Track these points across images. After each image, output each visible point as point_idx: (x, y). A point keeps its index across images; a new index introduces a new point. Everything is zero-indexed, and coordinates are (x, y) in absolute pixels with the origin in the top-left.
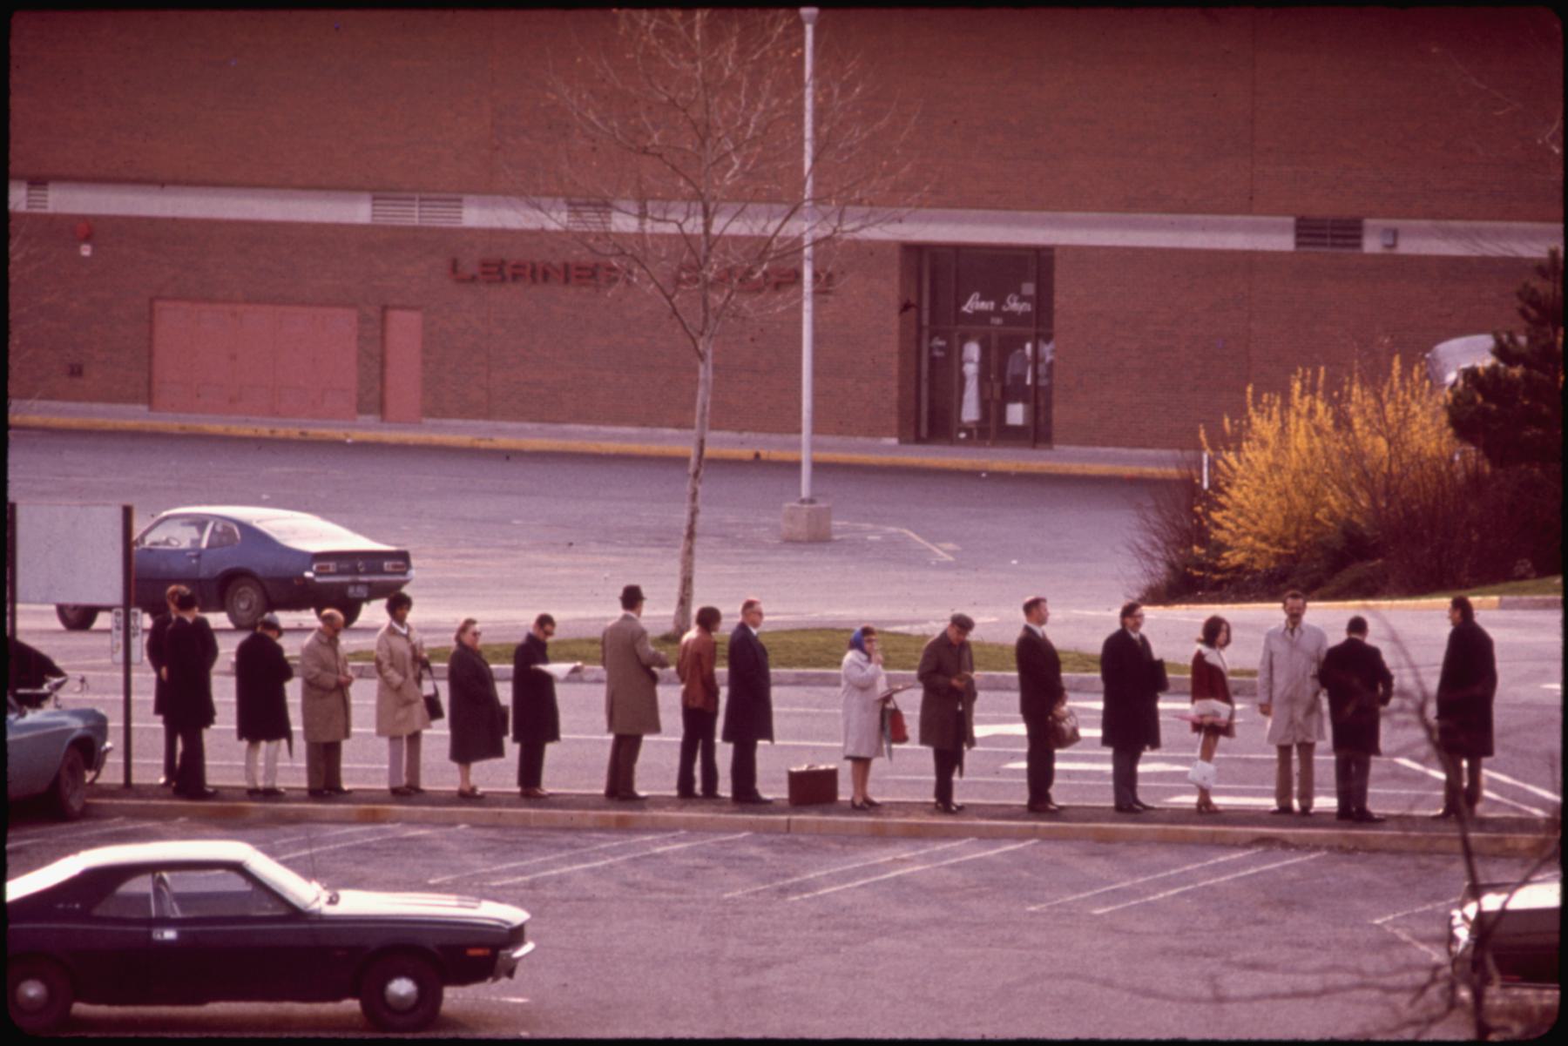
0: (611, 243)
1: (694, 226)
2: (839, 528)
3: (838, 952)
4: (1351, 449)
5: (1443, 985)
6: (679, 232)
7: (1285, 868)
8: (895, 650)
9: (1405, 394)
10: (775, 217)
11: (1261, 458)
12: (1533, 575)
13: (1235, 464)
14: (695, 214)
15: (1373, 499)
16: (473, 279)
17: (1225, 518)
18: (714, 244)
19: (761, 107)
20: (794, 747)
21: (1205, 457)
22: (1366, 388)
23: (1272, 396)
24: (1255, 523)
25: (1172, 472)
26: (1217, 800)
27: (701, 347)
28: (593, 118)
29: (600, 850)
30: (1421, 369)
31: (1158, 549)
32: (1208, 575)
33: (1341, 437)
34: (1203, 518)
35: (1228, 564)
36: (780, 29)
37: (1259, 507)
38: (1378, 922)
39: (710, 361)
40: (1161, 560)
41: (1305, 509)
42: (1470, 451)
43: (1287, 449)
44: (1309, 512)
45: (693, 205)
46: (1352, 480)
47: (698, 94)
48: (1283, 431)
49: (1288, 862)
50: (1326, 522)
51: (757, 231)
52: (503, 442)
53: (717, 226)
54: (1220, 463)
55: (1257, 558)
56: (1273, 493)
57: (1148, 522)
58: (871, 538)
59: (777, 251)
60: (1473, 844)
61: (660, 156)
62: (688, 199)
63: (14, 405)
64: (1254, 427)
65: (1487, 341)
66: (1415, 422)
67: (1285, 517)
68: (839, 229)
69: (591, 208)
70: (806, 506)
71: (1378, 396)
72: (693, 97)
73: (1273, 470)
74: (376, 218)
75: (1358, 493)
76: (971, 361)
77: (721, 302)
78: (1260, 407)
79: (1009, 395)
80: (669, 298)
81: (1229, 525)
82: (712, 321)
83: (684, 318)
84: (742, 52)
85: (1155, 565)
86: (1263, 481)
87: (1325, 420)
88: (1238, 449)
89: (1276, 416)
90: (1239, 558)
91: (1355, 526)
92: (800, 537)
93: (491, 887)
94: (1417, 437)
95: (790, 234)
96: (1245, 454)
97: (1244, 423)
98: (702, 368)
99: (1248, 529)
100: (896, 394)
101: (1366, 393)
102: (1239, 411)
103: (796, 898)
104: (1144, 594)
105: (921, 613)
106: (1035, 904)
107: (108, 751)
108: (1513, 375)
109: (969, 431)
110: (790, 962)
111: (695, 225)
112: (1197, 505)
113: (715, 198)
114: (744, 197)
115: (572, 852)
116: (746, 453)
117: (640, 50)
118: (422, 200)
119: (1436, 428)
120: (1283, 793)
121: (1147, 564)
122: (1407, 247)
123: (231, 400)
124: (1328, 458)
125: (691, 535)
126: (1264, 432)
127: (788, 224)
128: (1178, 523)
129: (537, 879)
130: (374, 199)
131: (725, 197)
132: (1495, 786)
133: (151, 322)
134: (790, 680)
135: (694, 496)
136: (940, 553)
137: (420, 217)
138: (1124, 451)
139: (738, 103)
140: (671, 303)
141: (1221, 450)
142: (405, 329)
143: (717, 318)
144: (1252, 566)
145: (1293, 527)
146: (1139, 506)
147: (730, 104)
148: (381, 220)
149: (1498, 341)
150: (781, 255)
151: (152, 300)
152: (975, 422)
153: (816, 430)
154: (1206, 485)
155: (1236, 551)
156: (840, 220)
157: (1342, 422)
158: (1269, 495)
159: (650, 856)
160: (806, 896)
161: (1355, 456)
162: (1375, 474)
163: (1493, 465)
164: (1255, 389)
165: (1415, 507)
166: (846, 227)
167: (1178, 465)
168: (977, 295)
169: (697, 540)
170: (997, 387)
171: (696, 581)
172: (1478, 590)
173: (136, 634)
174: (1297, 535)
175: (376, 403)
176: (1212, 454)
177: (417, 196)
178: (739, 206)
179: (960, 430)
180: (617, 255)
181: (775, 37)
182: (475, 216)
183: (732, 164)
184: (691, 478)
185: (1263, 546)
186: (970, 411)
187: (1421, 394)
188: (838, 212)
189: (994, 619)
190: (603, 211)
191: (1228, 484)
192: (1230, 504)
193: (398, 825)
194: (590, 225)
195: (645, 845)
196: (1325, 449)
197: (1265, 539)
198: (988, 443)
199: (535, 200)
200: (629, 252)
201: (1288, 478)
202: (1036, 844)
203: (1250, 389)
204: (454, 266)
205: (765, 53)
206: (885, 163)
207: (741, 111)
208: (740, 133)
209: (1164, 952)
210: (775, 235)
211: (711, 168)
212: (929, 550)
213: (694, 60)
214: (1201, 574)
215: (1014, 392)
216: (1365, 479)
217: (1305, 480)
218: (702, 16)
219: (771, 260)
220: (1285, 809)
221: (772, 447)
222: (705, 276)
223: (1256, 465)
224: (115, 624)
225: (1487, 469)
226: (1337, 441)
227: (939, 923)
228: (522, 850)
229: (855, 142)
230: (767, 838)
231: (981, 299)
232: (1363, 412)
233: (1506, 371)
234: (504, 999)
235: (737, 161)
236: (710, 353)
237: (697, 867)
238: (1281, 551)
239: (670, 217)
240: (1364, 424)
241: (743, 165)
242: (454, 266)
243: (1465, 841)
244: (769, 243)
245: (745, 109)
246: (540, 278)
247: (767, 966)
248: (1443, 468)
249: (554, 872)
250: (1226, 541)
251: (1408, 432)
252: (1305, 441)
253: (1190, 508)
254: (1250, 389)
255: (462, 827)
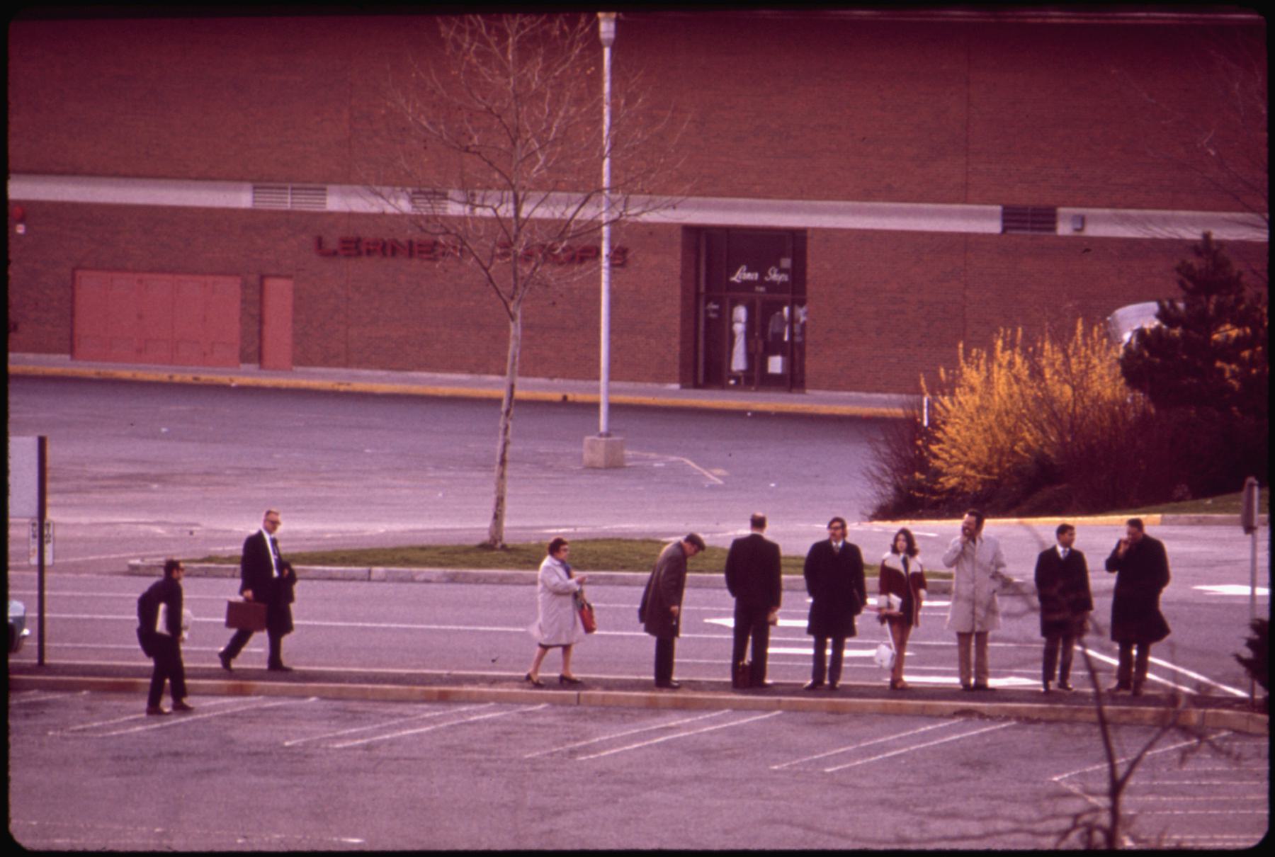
0: (439, 225)
1: (506, 211)
2: (631, 457)
3: (616, 802)
4: (1043, 395)
5: (1082, 830)
6: (494, 215)
7: (982, 735)
9: (1087, 349)
10: (572, 204)
11: (971, 402)
13: (949, 406)
15: (1061, 435)
16: (335, 253)
17: (940, 449)
18: (523, 225)
19: (561, 114)
21: (925, 400)
22: (1055, 346)
23: (980, 351)
24: (965, 454)
25: (899, 412)
26: (907, 678)
27: (511, 309)
28: (425, 123)
29: (424, 719)
31: (887, 475)
32: (927, 496)
33: (1035, 385)
34: (923, 449)
35: (943, 487)
36: (577, 51)
37: (969, 441)
38: (1056, 779)
39: (518, 321)
40: (890, 484)
41: (1005, 443)
42: (1139, 397)
43: (992, 395)
44: (1009, 445)
45: (506, 193)
46: (1044, 419)
47: (510, 104)
48: (988, 381)
49: (985, 730)
50: (1022, 453)
51: (557, 215)
52: (359, 386)
53: (525, 211)
54: (937, 405)
55: (967, 483)
56: (980, 429)
57: (879, 452)
58: (656, 465)
59: (574, 232)
61: (479, 153)
62: (502, 189)
63: (11, 356)
64: (965, 376)
65: (1153, 306)
66: (1095, 372)
67: (990, 449)
68: (624, 213)
69: (422, 196)
70: (604, 439)
71: (1064, 351)
72: (506, 106)
73: (981, 411)
74: (257, 204)
76: (739, 321)
78: (970, 359)
80: (486, 269)
81: (945, 456)
83: (498, 285)
84: (547, 69)
86: (972, 420)
87: (1022, 370)
88: (952, 394)
89: (983, 367)
90: (953, 482)
91: (1046, 457)
92: (597, 465)
94: (1096, 384)
95: (584, 218)
96: (957, 398)
97: (957, 372)
98: (512, 325)
99: (960, 459)
101: (1056, 349)
102: (952, 364)
103: (583, 758)
104: (876, 511)
106: (777, 764)
107: (24, 637)
108: (1174, 335)
110: (578, 810)
111: (507, 211)
113: (524, 188)
114: (548, 186)
115: (402, 720)
116: (557, 396)
117: (464, 67)
118: (293, 189)
119: (1112, 377)
121: (877, 486)
122: (1093, 231)
123: (139, 351)
124: (1025, 402)
125: (503, 462)
126: (972, 381)
127: (582, 210)
128: (903, 454)
129: (373, 742)
130: (255, 188)
131: (533, 187)
132: (1159, 670)
133: (72, 288)
137: (292, 203)
138: (864, 395)
139: (542, 112)
141: (937, 395)
142: (279, 293)
143: (525, 286)
144: (962, 489)
145: (996, 458)
146: (871, 441)
148: (260, 206)
149: (1162, 307)
150: (578, 234)
151: (74, 270)
152: (742, 371)
153: (612, 377)
154: (925, 423)
155: (949, 477)
156: (625, 207)
157: (1036, 373)
158: (977, 431)
160: (592, 756)
161: (1046, 401)
164: (965, 346)
165: (1094, 441)
167: (902, 406)
168: (744, 268)
169: (509, 466)
170: (761, 343)
171: (507, 501)
172: (1144, 509)
173: (48, 542)
174: (1000, 464)
175: (255, 354)
176: (930, 397)
177: (289, 186)
178: (542, 195)
180: (443, 234)
181: (573, 58)
182: (336, 202)
183: (538, 160)
184: (503, 417)
186: (738, 362)
187: (1100, 351)
188: (623, 199)
191: (944, 423)
192: (945, 438)
193: (260, 698)
194: (422, 210)
195: (460, 714)
196: (1022, 395)
197: (973, 467)
198: (753, 388)
199: (378, 189)
200: (453, 231)
201: (992, 417)
203: (961, 345)
204: (319, 242)
205: (564, 71)
207: (545, 117)
209: (882, 802)
211: (521, 164)
212: (703, 475)
213: (507, 77)
214: (922, 495)
215: (774, 346)
216: (1055, 418)
217: (1006, 419)
218: (513, 40)
220: (967, 687)
221: (577, 391)
222: (515, 251)
223: (967, 407)
224: (31, 533)
225: (1153, 411)
226: (1032, 388)
227: (698, 779)
228: (360, 719)
229: (638, 143)
230: (560, 709)
231: (748, 271)
232: (1052, 365)
234: (344, 840)
235: (541, 158)
236: (519, 314)
238: (987, 477)
239: (487, 203)
240: (1054, 374)
241: (546, 161)
242: (319, 242)
243: (1100, 713)
245: (549, 115)
246: (389, 252)
249: (387, 737)
250: (942, 468)
251: (1090, 381)
252: (1006, 388)
253: (913, 442)
254: (961, 345)
255: (313, 699)
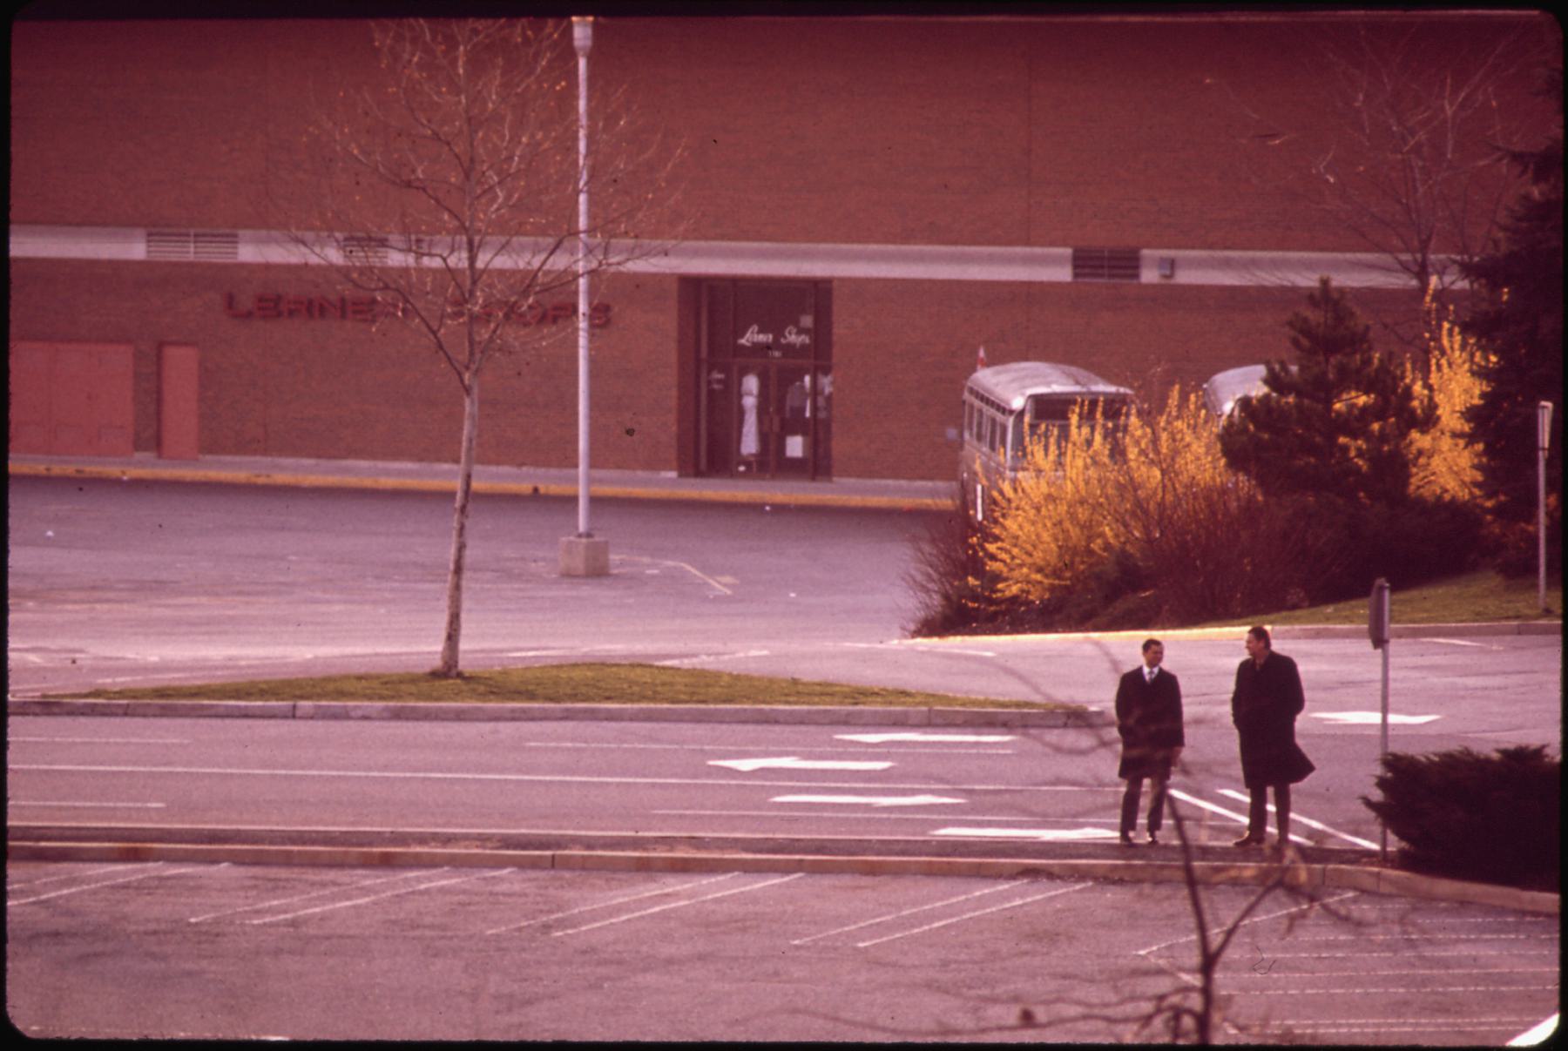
1: (459, 260)
3: (601, 987)
8: (664, 684)
10: (539, 252)
12: (1307, 604)
14: (460, 248)
15: (1146, 529)
16: (249, 315)
18: (480, 276)
20: (561, 782)
24: (1030, 555)
27: (467, 382)
30: (1197, 397)
37: (1034, 537)
38: (1142, 952)
40: (935, 592)
44: (1083, 543)
50: (1099, 552)
51: (522, 265)
52: (280, 478)
55: (1032, 589)
58: (649, 572)
59: (543, 284)
60: (1198, 873)
61: (424, 190)
65: (1261, 370)
68: (604, 262)
69: (355, 243)
75: (1133, 523)
76: (750, 394)
77: (486, 336)
79: (788, 428)
80: (434, 333)
81: (1004, 556)
82: (478, 356)
85: (930, 597)
89: (1053, 448)
93: (253, 926)
95: (555, 268)
98: (467, 402)
99: (1023, 561)
100: (674, 428)
103: (559, 934)
105: (693, 646)
108: (1287, 403)
109: (748, 464)
111: (460, 260)
112: (972, 537)
114: (509, 229)
115: (336, 889)
116: (525, 487)
120: (1128, 824)
121: (922, 596)
122: (1184, 277)
124: (1103, 488)
125: (458, 570)
127: (552, 259)
128: (953, 554)
129: (300, 916)
130: (150, 235)
134: (560, 715)
135: (462, 528)
136: (717, 585)
137: (195, 253)
138: (903, 483)
139: (502, 137)
140: (436, 337)
142: (182, 363)
146: (914, 539)
147: (495, 138)
149: (1271, 370)
153: (593, 463)
154: (980, 517)
155: (1011, 582)
156: (606, 252)
157: (1118, 452)
159: (413, 893)
160: (570, 931)
162: (1148, 504)
163: (1266, 494)
166: (613, 260)
168: (755, 328)
171: (463, 616)
175: (153, 440)
177: (192, 231)
178: (503, 239)
179: (739, 464)
182: (248, 253)
185: (1039, 577)
186: (750, 444)
189: (765, 652)
190: (367, 246)
191: (1004, 516)
197: (1040, 570)
198: (768, 476)
199: (299, 234)
202: (800, 878)
204: (230, 301)
206: (650, 196)
208: (505, 167)
210: (540, 269)
219: (536, 293)
221: (549, 481)
231: (760, 332)
233: (1278, 402)
235: (501, 194)
237: (460, 904)
238: (1057, 582)
241: (508, 197)
242: (230, 301)
244: (536, 275)
245: (509, 142)
247: (529, 1002)
248: (1215, 496)
